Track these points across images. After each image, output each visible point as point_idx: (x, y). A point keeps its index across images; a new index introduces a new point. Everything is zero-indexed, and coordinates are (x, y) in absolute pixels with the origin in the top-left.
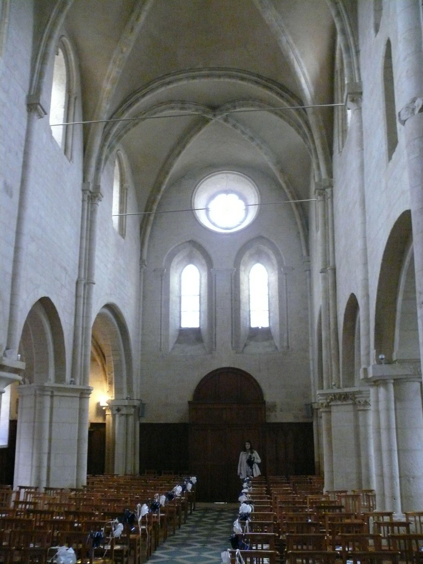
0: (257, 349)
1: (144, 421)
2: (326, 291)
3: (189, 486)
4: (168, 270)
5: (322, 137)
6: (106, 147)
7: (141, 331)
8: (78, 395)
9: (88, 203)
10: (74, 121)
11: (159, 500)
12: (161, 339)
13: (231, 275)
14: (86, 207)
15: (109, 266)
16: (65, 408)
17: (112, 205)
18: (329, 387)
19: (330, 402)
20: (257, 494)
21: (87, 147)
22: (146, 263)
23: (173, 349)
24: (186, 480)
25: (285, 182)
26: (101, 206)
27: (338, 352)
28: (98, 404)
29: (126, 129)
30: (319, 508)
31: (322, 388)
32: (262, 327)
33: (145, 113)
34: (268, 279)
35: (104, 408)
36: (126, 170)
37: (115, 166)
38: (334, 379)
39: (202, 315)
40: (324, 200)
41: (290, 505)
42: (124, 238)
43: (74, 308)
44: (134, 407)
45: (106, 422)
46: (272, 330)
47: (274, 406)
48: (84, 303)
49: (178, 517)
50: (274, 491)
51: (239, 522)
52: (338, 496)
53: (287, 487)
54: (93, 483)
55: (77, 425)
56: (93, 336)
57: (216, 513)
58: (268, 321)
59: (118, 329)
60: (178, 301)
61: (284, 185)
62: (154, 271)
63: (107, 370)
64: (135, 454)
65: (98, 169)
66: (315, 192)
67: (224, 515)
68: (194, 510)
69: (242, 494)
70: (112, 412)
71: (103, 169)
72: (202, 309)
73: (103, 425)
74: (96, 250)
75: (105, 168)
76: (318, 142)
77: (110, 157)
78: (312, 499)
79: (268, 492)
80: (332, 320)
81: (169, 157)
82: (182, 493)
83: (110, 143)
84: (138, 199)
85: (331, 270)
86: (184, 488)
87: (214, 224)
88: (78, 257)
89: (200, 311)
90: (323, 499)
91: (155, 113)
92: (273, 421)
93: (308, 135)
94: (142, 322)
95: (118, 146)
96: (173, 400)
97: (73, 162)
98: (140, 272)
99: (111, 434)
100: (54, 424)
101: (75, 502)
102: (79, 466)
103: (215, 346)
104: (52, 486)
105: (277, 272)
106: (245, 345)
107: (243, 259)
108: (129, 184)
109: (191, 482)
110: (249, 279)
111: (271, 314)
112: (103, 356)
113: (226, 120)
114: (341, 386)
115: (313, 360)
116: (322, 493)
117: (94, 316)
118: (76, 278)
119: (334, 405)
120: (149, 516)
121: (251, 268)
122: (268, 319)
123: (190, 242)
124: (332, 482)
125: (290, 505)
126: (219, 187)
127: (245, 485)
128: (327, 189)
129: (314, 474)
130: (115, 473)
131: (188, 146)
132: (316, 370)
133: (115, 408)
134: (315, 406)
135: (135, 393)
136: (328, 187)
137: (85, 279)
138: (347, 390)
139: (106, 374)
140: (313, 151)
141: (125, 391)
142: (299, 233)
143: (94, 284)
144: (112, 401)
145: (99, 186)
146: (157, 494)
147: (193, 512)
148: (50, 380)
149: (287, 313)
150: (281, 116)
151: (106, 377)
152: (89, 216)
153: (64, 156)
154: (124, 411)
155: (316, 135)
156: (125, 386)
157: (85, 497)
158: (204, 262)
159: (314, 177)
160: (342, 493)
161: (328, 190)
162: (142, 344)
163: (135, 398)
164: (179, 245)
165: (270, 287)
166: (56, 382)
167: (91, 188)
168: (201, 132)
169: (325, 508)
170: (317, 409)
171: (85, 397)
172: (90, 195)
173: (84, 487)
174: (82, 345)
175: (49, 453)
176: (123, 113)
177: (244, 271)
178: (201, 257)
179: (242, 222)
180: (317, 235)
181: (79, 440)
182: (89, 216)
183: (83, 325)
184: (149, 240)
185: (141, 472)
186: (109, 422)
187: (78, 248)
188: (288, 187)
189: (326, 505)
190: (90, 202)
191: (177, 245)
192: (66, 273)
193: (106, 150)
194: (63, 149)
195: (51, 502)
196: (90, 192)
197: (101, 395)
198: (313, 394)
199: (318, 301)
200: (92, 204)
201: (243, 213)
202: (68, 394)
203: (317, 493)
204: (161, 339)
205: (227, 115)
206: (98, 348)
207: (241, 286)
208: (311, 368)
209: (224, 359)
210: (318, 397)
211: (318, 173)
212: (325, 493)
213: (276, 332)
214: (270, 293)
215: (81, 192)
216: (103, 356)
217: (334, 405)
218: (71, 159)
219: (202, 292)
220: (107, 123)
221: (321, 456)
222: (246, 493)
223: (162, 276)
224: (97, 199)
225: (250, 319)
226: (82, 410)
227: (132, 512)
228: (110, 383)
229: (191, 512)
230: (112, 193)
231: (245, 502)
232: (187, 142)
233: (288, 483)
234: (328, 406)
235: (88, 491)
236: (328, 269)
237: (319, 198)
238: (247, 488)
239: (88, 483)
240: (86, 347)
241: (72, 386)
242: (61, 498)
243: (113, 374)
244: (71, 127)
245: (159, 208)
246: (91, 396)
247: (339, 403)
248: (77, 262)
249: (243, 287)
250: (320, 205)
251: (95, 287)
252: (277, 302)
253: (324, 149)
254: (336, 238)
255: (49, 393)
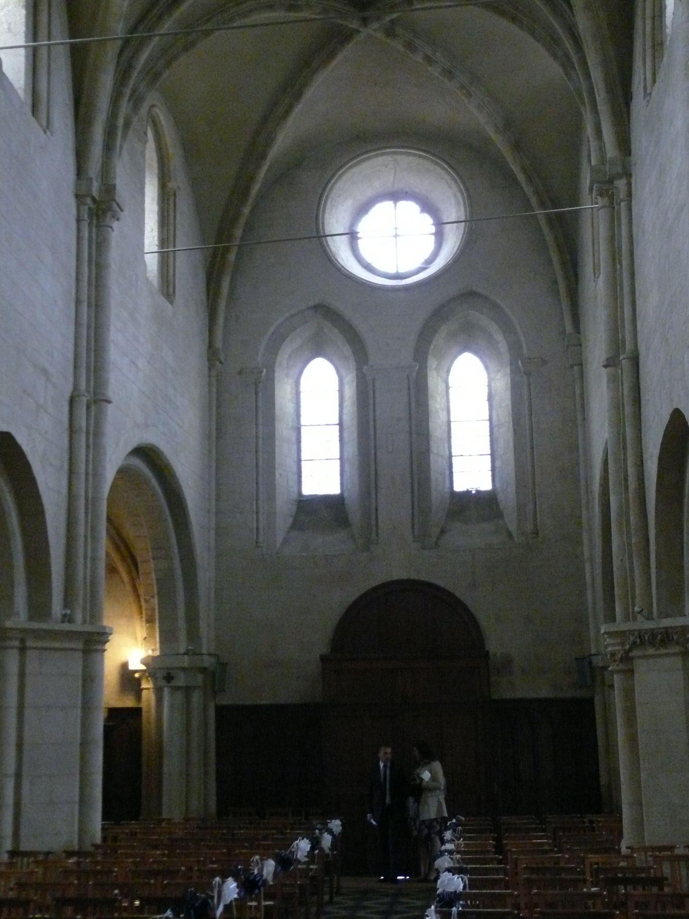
0: (470, 537)
1: (225, 700)
2: (617, 406)
3: (327, 841)
4: (271, 369)
5: (605, 64)
6: (126, 98)
7: (213, 503)
8: (81, 646)
9: (90, 224)
10: (49, 39)
11: (261, 870)
12: (257, 521)
13: (408, 377)
14: (86, 234)
15: (141, 363)
16: (51, 675)
17: (145, 229)
18: (627, 618)
19: (630, 650)
20: (476, 852)
21: (84, 101)
22: (222, 356)
23: (285, 541)
24: (319, 826)
25: (524, 169)
26: (117, 231)
27: (648, 540)
28: (125, 666)
29: (167, 56)
30: (615, 881)
31: (611, 617)
32: (478, 492)
33: (208, 20)
34: (489, 386)
35: (137, 675)
36: (171, 151)
37: (146, 142)
38: (637, 600)
39: (347, 468)
40: (612, 206)
41: (548, 876)
42: (171, 302)
43: (66, 456)
44: (203, 670)
45: (143, 705)
46: (500, 497)
47: (507, 663)
48: (88, 446)
49: (303, 910)
50: (510, 844)
51: (436, 912)
52: (655, 857)
53: (541, 838)
54: (115, 839)
55: (79, 712)
56: (109, 520)
57: (386, 900)
58: (490, 478)
59: (163, 501)
60: (294, 439)
61: (521, 177)
62: (240, 373)
63: (141, 591)
64: (206, 774)
65: (109, 148)
66: (591, 189)
67: (403, 903)
68: (338, 893)
69: (442, 853)
70: (155, 684)
71: (121, 147)
72: (346, 455)
73: (136, 712)
74: (112, 328)
75: (125, 146)
76: (597, 75)
77: (135, 120)
78: (597, 863)
79: (499, 848)
80: (631, 471)
81: (265, 119)
82: (311, 854)
83: (134, 91)
84: (200, 209)
85: (627, 361)
86: (316, 844)
87: (368, 267)
88: (71, 347)
89: (341, 459)
90: (622, 864)
91: (232, 19)
92: (508, 695)
93: (575, 59)
94: (217, 484)
95: (153, 98)
96: (289, 653)
97: (52, 133)
98: (210, 377)
99: (153, 726)
100: (28, 713)
101: (78, 879)
102: (84, 802)
103: (377, 535)
104: (24, 847)
105: (508, 370)
106: (443, 532)
107: (434, 342)
108: (179, 181)
109: (330, 832)
110: (447, 388)
111: (498, 464)
112: (132, 562)
113: (390, 32)
114: (655, 615)
115: (591, 560)
116: (619, 851)
117: (110, 474)
118: (68, 389)
119: (639, 657)
120: (240, 902)
121: (452, 362)
122: (490, 473)
123: (316, 308)
124: (639, 824)
125: (548, 876)
126: (377, 185)
127: (448, 835)
128: (617, 182)
129: (599, 811)
130: (165, 816)
131: (309, 94)
132: (599, 581)
133: (160, 675)
134: (598, 661)
135: (204, 640)
136: (619, 176)
137: (88, 392)
138: (667, 623)
139: (139, 601)
140: (585, 95)
141: (183, 635)
142: (555, 282)
143: (109, 402)
144: (154, 658)
145: (114, 186)
146: (257, 857)
147: (336, 899)
148: (18, 614)
149: (533, 459)
150: (514, 19)
151: (140, 607)
152: (94, 253)
153: (33, 119)
154: (181, 680)
155: (593, 59)
156: (182, 623)
157: (99, 868)
158: (347, 350)
159: (589, 156)
160: (663, 852)
161: (621, 184)
162: (217, 534)
163: (204, 651)
164: (292, 316)
165: (495, 403)
166: (31, 618)
167: (95, 193)
168: (334, 63)
169: (625, 882)
170: (605, 668)
171: (97, 651)
172: (92, 206)
173: (97, 846)
174: (86, 537)
175: (18, 775)
176: (160, 18)
177: (437, 369)
178: (340, 340)
179: (429, 262)
180: (596, 288)
181: (85, 744)
182: (94, 253)
183: (86, 492)
184: (227, 306)
185: (220, 813)
186: (149, 706)
187: (72, 328)
188: (530, 179)
189: (629, 875)
190: (95, 222)
191: (287, 315)
192: (48, 380)
193: (125, 107)
194: (29, 102)
195: (23, 880)
196: (94, 199)
197: (131, 648)
198: (592, 634)
199: (600, 430)
200: (98, 226)
201: (431, 242)
202: (57, 645)
203: (607, 851)
204: (257, 521)
205: (392, 21)
206: (122, 545)
207: (431, 402)
208: (588, 579)
209: (397, 563)
210: (603, 639)
211: (597, 146)
212: (624, 850)
213: (508, 501)
214: (495, 418)
215: (72, 202)
216: (132, 562)
217: (639, 657)
218: (47, 127)
219: (345, 417)
220: (126, 42)
221: (614, 772)
222: (450, 852)
223: (256, 384)
224: (109, 214)
225: (451, 473)
226: (90, 678)
227: (203, 896)
228: (150, 621)
229: (331, 898)
230: (143, 202)
231: (449, 870)
232: (305, 85)
233: (543, 830)
234: (627, 658)
235: (105, 854)
236: (621, 358)
237: (601, 201)
238: (452, 841)
239: (104, 839)
240: (95, 539)
241: (66, 627)
242: (44, 874)
243: (155, 601)
244: (43, 53)
245: (250, 246)
246: (107, 646)
247: (651, 651)
248: (71, 356)
249: (436, 404)
250: (602, 217)
251: (110, 409)
252: (510, 436)
253: (610, 90)
254: (638, 288)
255: (17, 643)
